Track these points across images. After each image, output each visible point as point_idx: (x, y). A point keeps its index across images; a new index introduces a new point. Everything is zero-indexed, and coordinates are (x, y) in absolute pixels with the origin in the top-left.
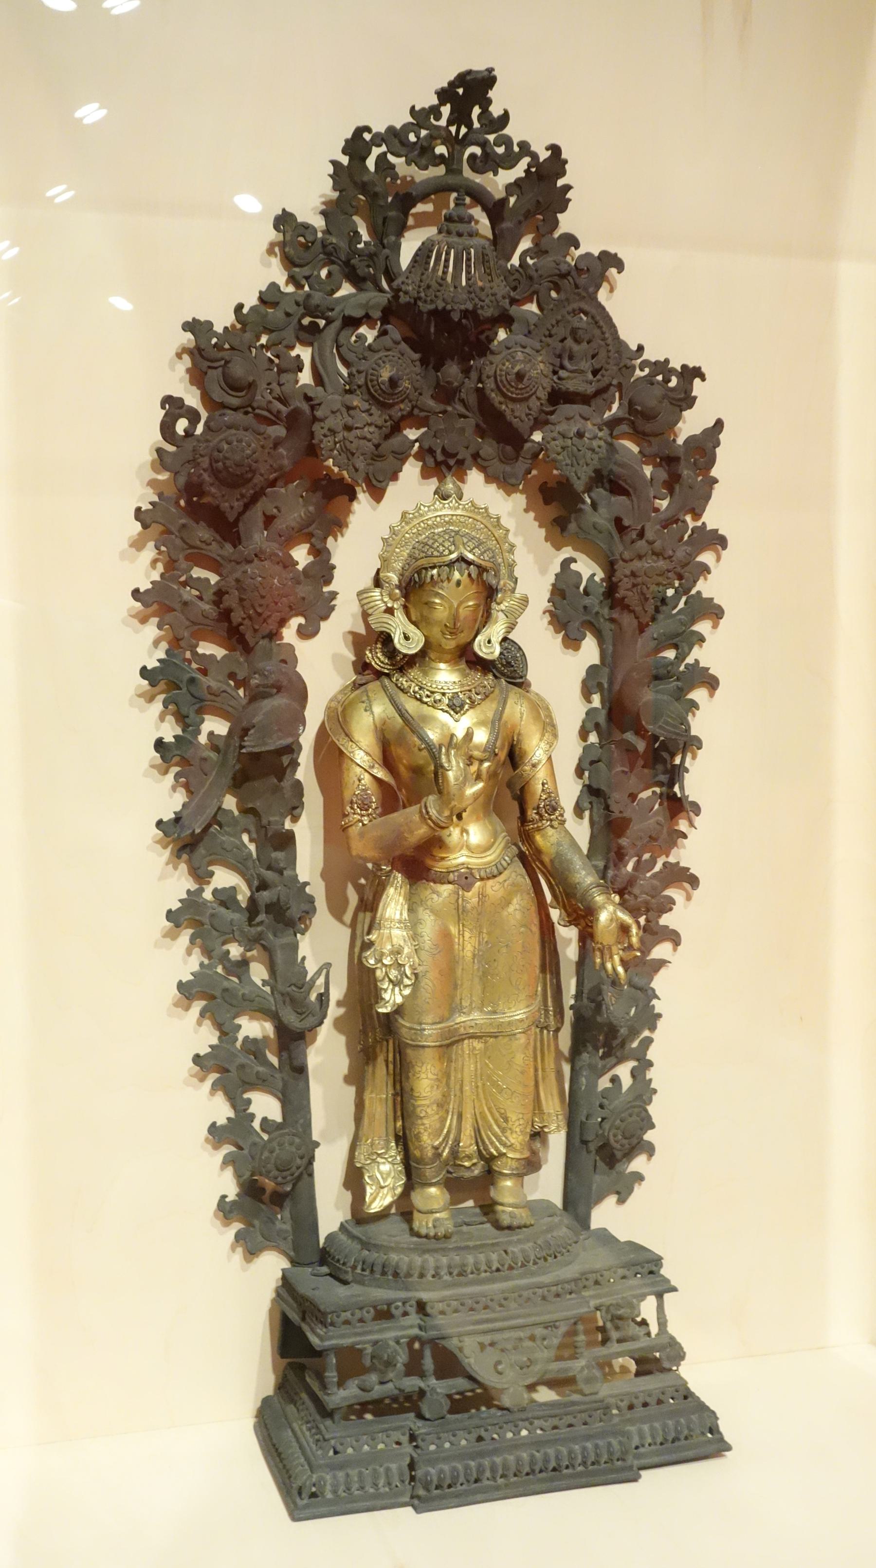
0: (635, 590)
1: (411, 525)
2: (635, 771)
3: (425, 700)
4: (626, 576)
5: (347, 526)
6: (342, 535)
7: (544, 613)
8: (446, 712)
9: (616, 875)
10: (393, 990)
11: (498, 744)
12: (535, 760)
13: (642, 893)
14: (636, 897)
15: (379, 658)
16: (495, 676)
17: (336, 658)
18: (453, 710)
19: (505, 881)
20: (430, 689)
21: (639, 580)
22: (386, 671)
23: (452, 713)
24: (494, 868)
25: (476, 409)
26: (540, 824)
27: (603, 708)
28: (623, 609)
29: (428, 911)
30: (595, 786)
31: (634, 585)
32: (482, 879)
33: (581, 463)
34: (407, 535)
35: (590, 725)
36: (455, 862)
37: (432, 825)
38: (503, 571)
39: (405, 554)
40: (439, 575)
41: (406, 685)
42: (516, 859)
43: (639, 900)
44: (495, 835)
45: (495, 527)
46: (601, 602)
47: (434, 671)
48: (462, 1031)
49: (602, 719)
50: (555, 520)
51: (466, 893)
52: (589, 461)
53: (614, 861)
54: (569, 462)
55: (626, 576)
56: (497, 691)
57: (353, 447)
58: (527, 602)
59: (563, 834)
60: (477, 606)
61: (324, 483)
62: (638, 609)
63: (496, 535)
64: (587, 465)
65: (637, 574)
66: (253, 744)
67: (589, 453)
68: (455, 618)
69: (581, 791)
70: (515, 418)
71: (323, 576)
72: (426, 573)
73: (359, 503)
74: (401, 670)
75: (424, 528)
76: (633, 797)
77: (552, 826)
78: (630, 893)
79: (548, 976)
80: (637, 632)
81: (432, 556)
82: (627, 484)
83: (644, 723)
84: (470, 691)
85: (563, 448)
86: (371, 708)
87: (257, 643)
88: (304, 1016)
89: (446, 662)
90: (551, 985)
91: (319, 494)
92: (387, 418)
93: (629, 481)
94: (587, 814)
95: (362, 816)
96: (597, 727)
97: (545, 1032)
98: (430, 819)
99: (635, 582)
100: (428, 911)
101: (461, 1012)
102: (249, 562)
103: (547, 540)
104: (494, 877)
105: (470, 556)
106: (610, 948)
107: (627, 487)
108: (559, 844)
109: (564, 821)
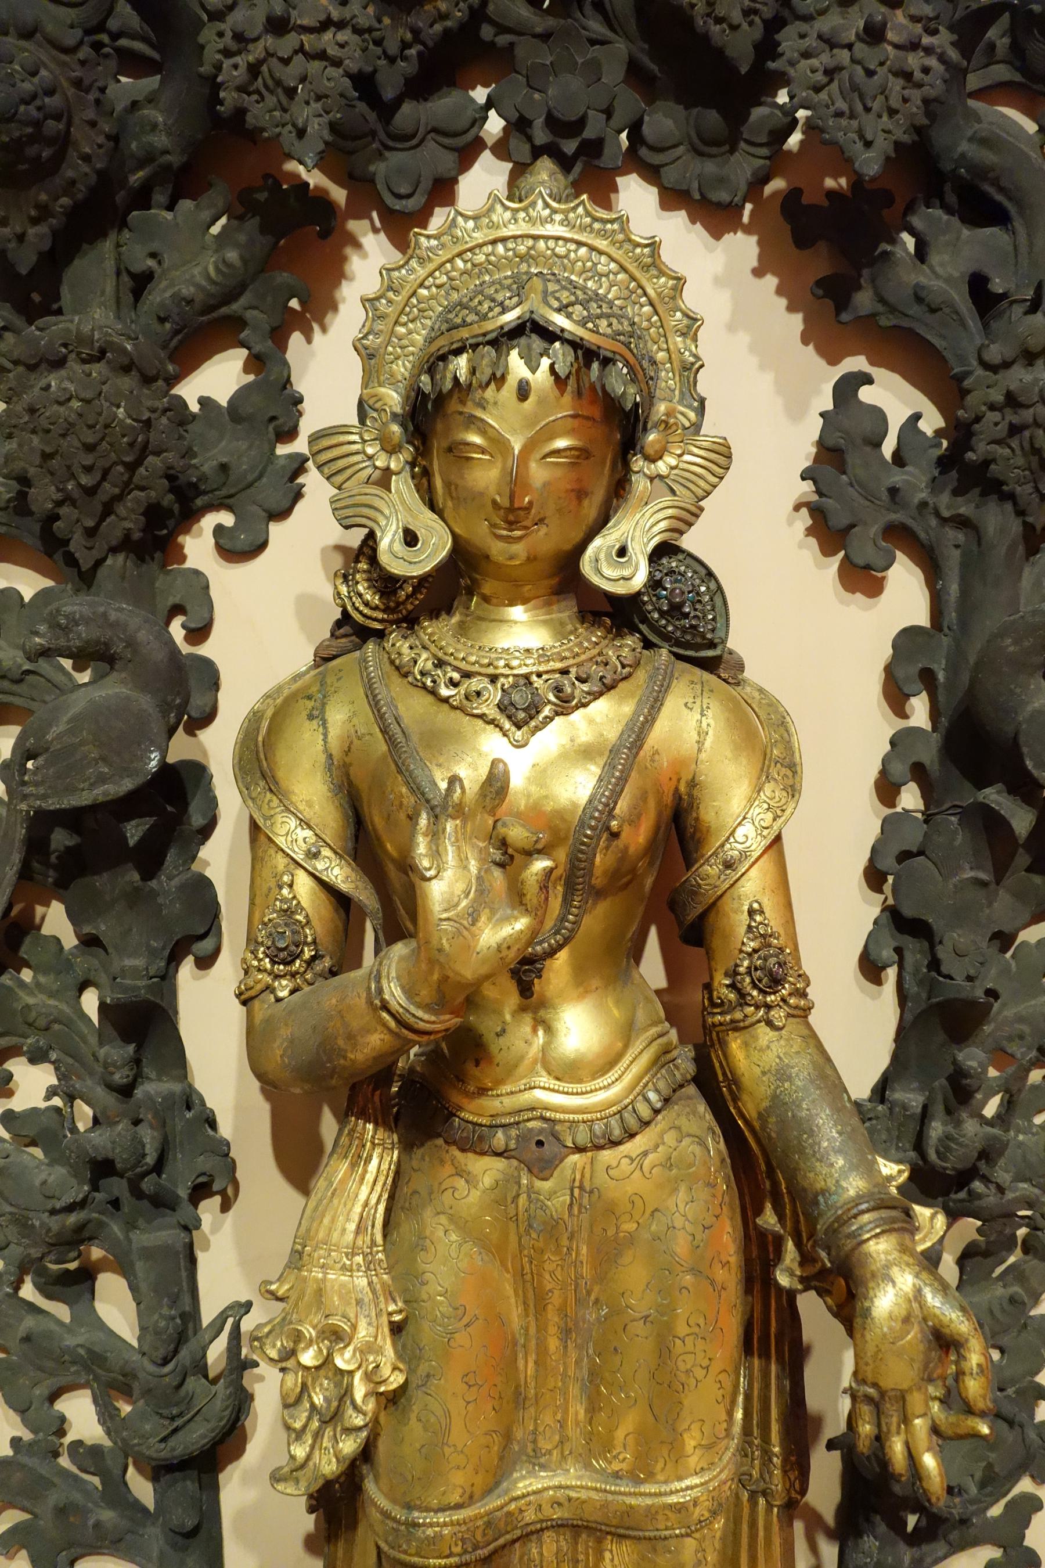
0: (1015, 443)
1: (431, 266)
2: (1008, 881)
3: (444, 692)
4: (992, 407)
5: (335, 308)
6: (324, 329)
7: (797, 508)
8: (492, 722)
9: (948, 1137)
10: (317, 1435)
11: (622, 806)
12: (732, 850)
13: (1020, 1178)
14: (1001, 1190)
15: (360, 595)
16: (648, 645)
17: (305, 603)
18: (509, 717)
19: (645, 1154)
20: (462, 665)
21: (1027, 415)
22: (378, 626)
23: (507, 725)
24: (614, 1122)
25: (632, 26)
26: (738, 1015)
27: (935, 728)
28: (984, 494)
29: (443, 1219)
30: (908, 911)
31: (1014, 430)
32: (580, 1150)
33: (876, 105)
34: (424, 292)
35: (900, 769)
36: (509, 1103)
37: (392, 1024)
38: (668, 380)
39: (419, 339)
40: (473, 371)
41: (407, 654)
42: (692, 1090)
43: (1010, 1195)
44: (627, 1032)
45: (645, 268)
46: (934, 479)
47: (484, 625)
48: (530, 1516)
49: (929, 755)
50: (819, 283)
51: (538, 1184)
52: (895, 103)
53: (946, 1101)
54: (841, 105)
55: (992, 407)
56: (641, 675)
57: (289, 75)
58: (729, 457)
59: (797, 1044)
60: (581, 454)
61: (262, 196)
62: (1024, 491)
63: (650, 291)
64: (892, 112)
65: (1022, 399)
66: (41, 790)
67: (896, 85)
68: (515, 482)
69: (876, 922)
70: (719, 21)
71: (273, 419)
72: (445, 368)
73: (365, 256)
74: (410, 622)
75: (465, 272)
76: (1004, 939)
77: (769, 1023)
78: (986, 1180)
79: (773, 1368)
80: (1021, 549)
81: (464, 324)
82: (1001, 189)
83: (1029, 764)
84: (565, 672)
85: (830, 73)
86: (323, 711)
87: (99, 563)
88: (179, 1422)
89: (524, 601)
90: (780, 1390)
91: (253, 223)
92: (409, 36)
93: (1004, 183)
94: (891, 974)
95: (277, 977)
96: (919, 773)
97: (762, 1501)
98: (385, 1007)
99: (1016, 420)
100: (443, 1219)
101: (536, 1460)
102: (59, 363)
103: (805, 339)
104: (615, 1144)
105: (560, 321)
106: (902, 1397)
107: (999, 197)
108: (782, 1074)
109: (807, 1010)
